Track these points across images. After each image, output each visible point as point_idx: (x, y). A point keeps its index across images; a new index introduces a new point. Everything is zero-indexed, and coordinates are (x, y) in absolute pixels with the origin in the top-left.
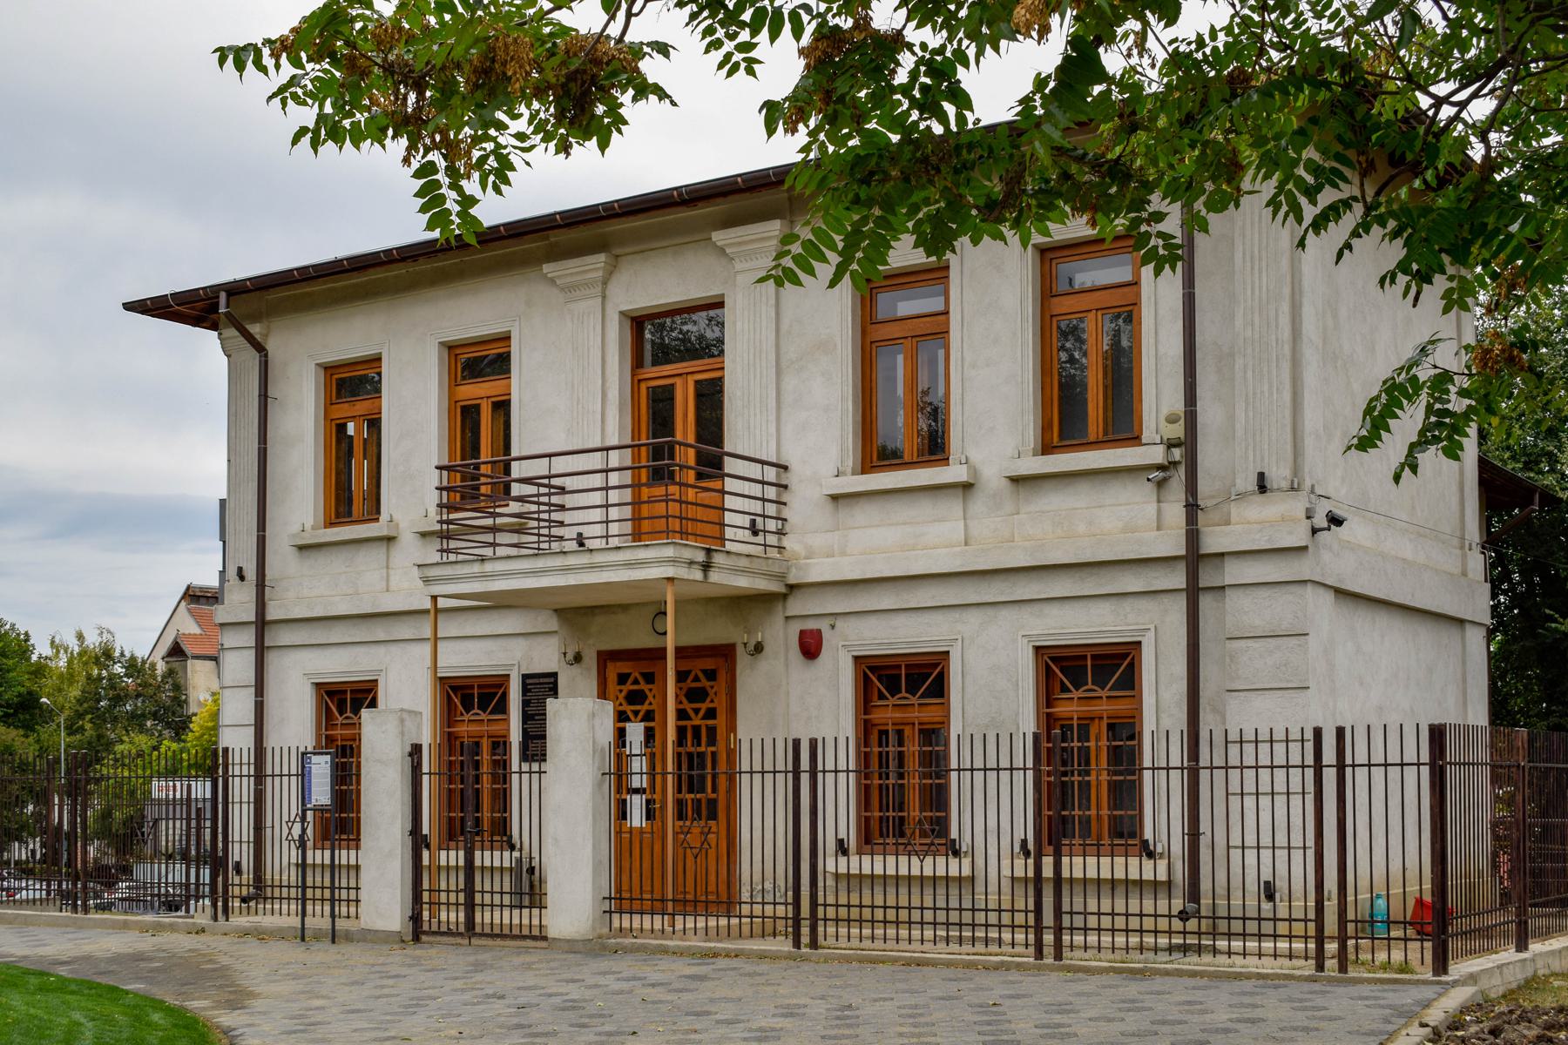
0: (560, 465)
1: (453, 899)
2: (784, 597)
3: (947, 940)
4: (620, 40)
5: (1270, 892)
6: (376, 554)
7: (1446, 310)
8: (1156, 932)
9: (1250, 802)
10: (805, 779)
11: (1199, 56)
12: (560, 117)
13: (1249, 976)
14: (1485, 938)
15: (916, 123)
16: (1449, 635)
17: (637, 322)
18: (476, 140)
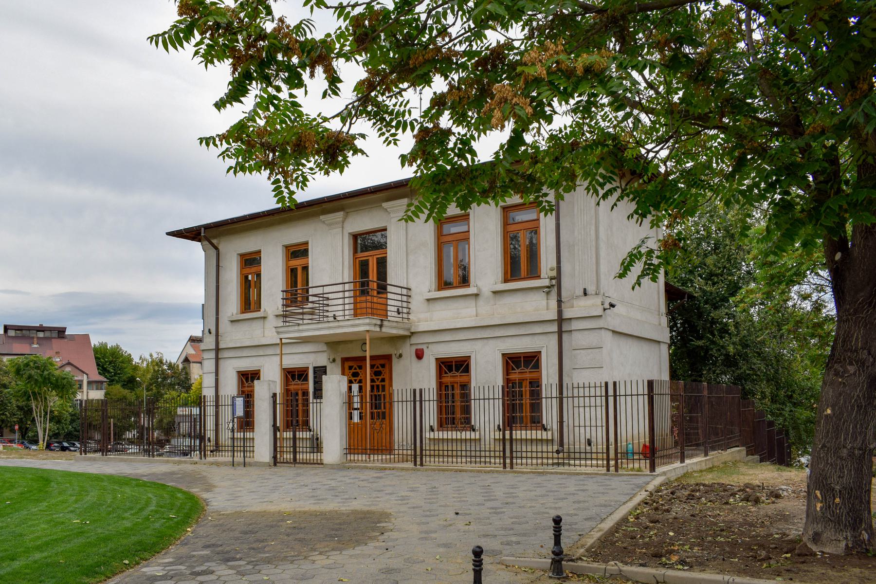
0: (327, 290)
2: (410, 337)
5: (589, 443)
7: (652, 227)
9: (582, 409)
10: (418, 404)
12: (325, 161)
13: (582, 474)
16: (654, 347)
17: (355, 237)
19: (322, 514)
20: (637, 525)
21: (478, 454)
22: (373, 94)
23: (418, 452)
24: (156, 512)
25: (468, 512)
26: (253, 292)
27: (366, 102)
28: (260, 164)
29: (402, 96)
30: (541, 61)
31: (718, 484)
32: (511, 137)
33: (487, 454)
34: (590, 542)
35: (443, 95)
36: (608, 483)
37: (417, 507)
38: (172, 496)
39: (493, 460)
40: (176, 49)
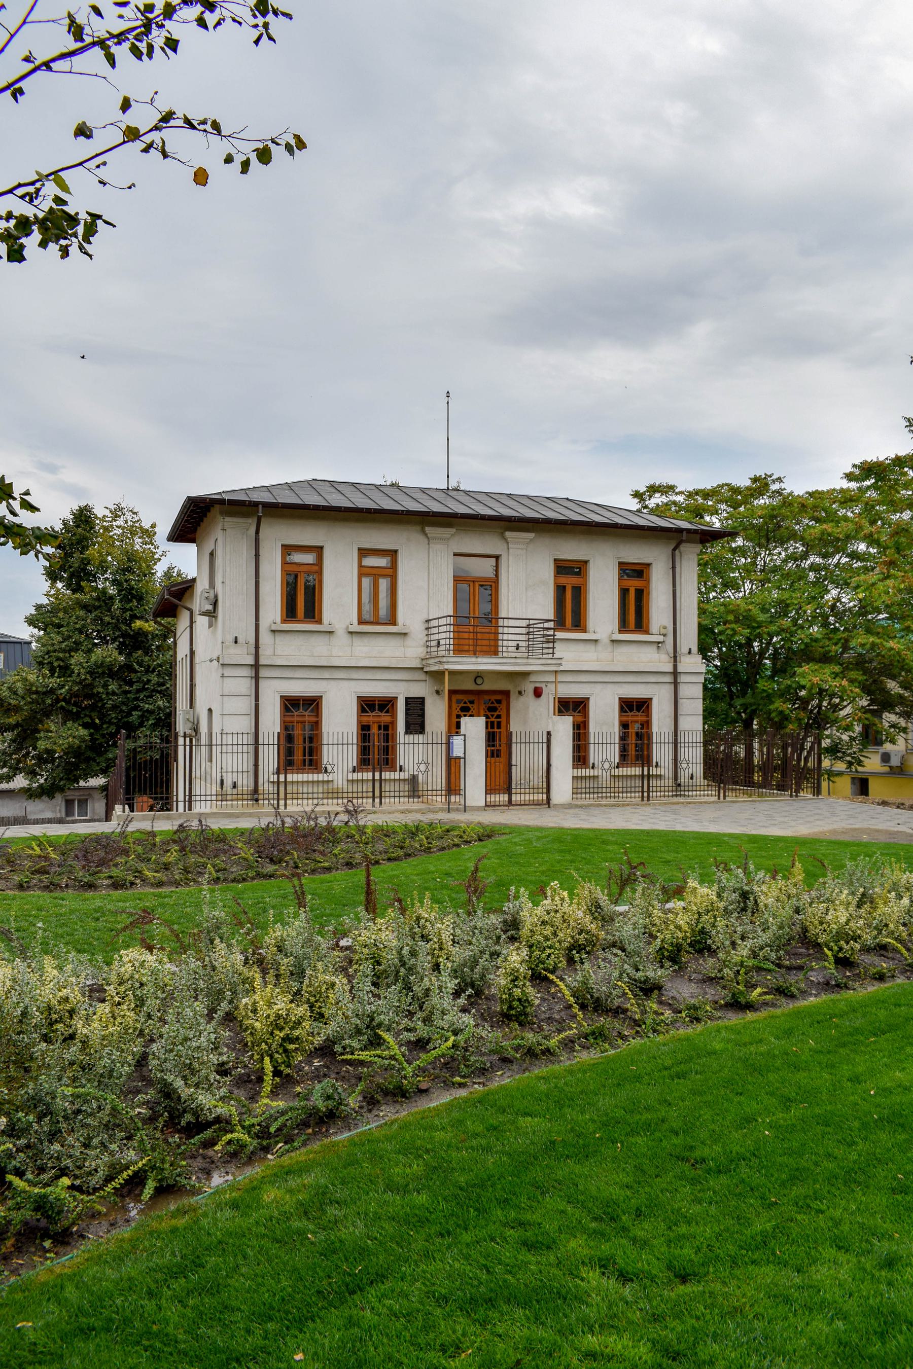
5: (235, 786)
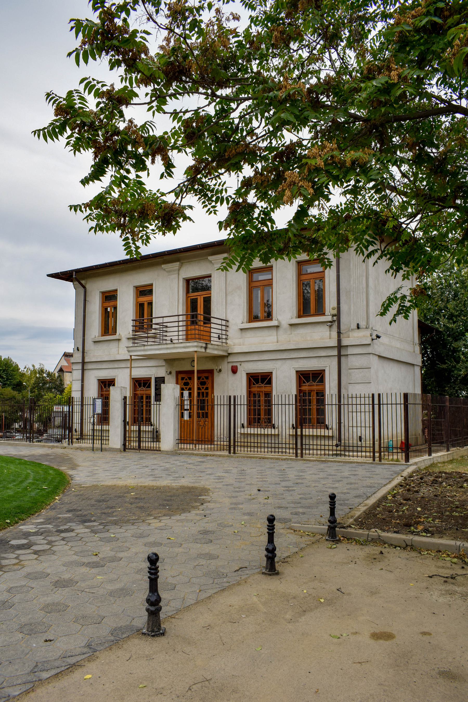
0: (166, 320)
1: (135, 439)
2: (227, 356)
3: (271, 452)
4: (180, 204)
6: (115, 344)
7: (403, 280)
8: (329, 450)
9: (354, 414)
10: (232, 407)
11: (337, 210)
12: (163, 225)
13: (354, 463)
14: (419, 452)
15: (260, 228)
16: (410, 369)
17: (188, 281)
18: (140, 231)
19: (158, 488)
20: (393, 502)
21: (277, 445)
22: (199, 176)
23: (232, 444)
24: (33, 484)
25: (267, 489)
26: (111, 321)
27: (194, 181)
28: (115, 226)
29: (220, 179)
30: (320, 156)
31: (456, 472)
32: (298, 210)
33: (284, 446)
34: (357, 514)
35: (250, 178)
36: (373, 469)
37: (229, 485)
38: (46, 472)
39: (288, 451)
40: (53, 140)
